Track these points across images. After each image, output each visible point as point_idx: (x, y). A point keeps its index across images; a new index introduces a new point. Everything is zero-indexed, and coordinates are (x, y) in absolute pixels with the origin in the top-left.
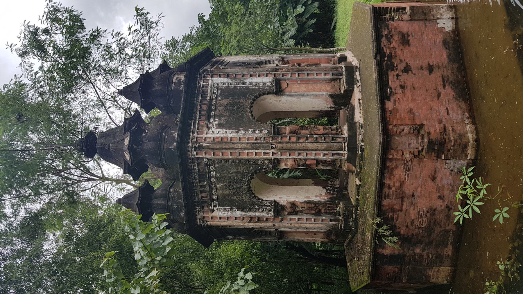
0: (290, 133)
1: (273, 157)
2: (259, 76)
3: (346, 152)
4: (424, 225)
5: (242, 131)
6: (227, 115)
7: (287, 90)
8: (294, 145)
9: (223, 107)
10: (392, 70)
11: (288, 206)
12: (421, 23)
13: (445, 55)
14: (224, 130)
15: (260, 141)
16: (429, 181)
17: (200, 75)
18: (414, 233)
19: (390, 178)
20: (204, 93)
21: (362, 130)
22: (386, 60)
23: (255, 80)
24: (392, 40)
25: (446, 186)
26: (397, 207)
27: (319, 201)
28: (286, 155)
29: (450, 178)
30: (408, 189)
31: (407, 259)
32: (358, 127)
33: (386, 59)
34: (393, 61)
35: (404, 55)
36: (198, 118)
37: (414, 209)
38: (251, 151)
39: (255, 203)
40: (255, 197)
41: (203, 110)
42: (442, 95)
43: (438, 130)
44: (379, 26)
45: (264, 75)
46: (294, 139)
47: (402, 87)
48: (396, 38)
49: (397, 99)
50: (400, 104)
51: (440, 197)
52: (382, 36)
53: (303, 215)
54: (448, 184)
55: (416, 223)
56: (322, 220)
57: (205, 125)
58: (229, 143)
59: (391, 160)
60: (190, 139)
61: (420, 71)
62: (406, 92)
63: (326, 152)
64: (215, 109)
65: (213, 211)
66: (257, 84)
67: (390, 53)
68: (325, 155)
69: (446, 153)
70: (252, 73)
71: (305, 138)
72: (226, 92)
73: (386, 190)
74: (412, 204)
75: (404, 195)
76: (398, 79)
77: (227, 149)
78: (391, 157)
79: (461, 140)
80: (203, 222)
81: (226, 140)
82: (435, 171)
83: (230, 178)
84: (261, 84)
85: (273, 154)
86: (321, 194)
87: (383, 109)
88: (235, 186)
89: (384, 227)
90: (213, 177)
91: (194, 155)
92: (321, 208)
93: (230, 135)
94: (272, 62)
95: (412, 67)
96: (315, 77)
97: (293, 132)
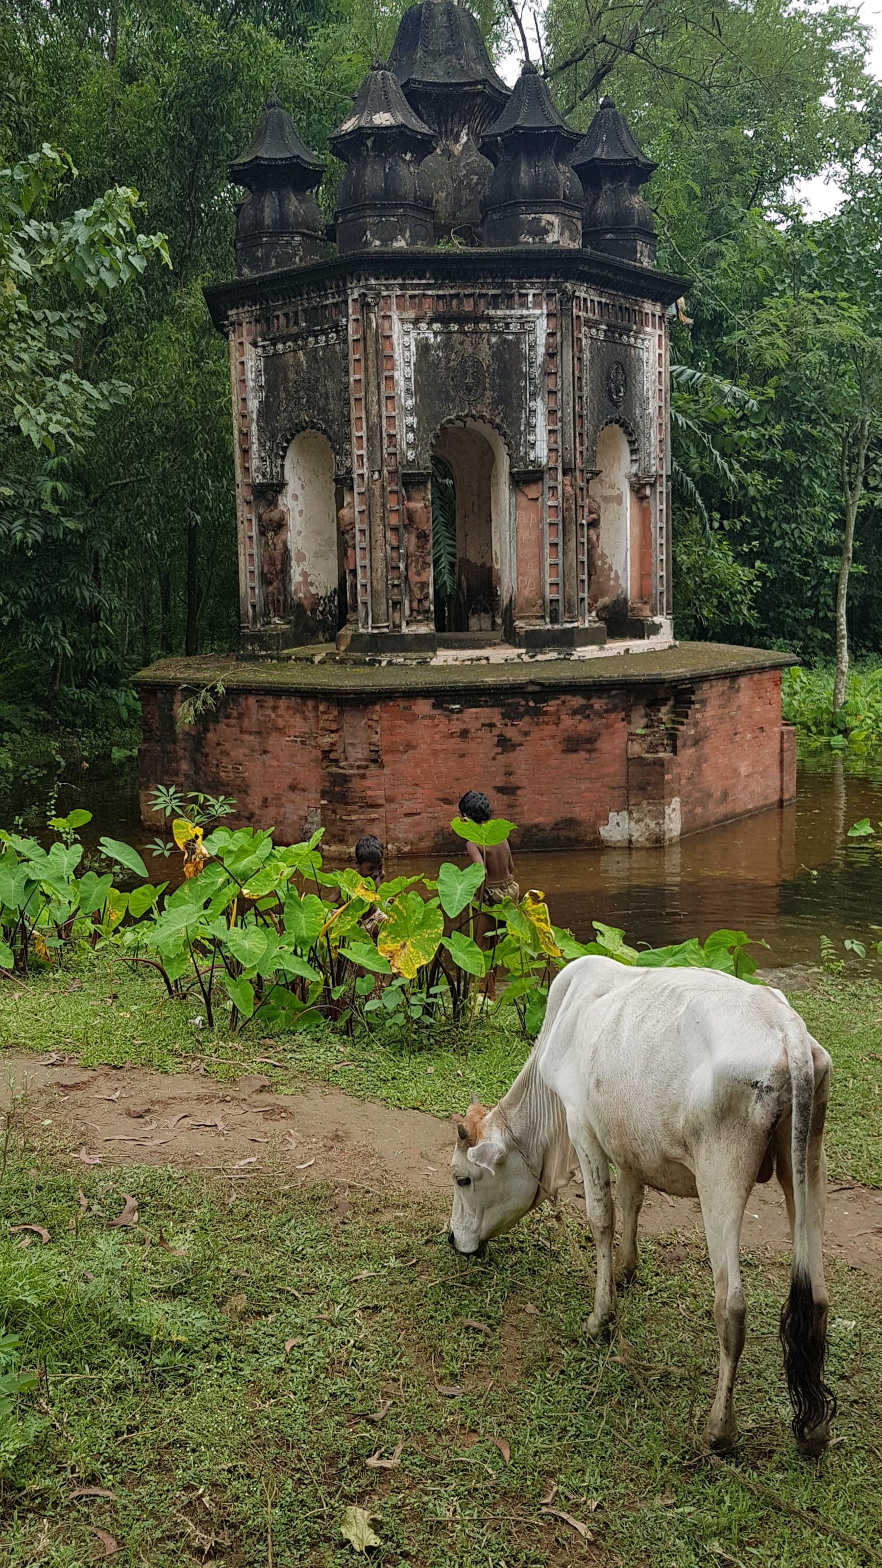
0: (408, 510)
1: (355, 476)
2: (550, 431)
3: (370, 630)
4: (222, 774)
5: (410, 403)
6: (452, 363)
7: (523, 501)
8: (378, 521)
9: (470, 350)
10: (504, 716)
11: (275, 515)
12: (621, 780)
13: (540, 820)
14: (413, 360)
15: (385, 446)
16: (288, 781)
17: (555, 285)
18: (209, 758)
19: (288, 708)
20: (507, 299)
21: (414, 663)
22: (527, 704)
23: (541, 422)
24: (579, 717)
25: (283, 810)
26: (246, 723)
27: (290, 580)
28: (360, 504)
29: (295, 818)
30: (274, 742)
31: (170, 747)
32: (423, 655)
33: (531, 704)
34: (526, 719)
35: (539, 741)
36: (440, 292)
37: (245, 755)
38: (364, 425)
39: (278, 440)
40: (288, 441)
41: (461, 302)
42: (446, 806)
43: (369, 793)
44: (614, 692)
45: (555, 442)
46: (394, 520)
47: (464, 734)
48: (584, 727)
49: (436, 721)
50: (426, 727)
51: (265, 800)
52: (589, 699)
53: (259, 546)
54: (285, 814)
55: (225, 760)
56: (253, 588)
57: (422, 313)
58: (378, 375)
59: (316, 708)
60: (386, 279)
61: (502, 770)
62: (453, 741)
63: (369, 588)
64: (465, 333)
65: (255, 345)
66: (531, 428)
67: (546, 713)
68: (364, 586)
69: (330, 807)
70: (559, 414)
71: (395, 544)
72: (510, 355)
73: (270, 701)
74: (252, 751)
75: (265, 735)
76: (483, 725)
77: (366, 370)
78: (322, 708)
79: (352, 832)
80: (232, 324)
81: (386, 365)
82: (304, 790)
83: (317, 380)
84: (531, 438)
85: (361, 476)
86: (312, 584)
87: (413, 694)
88: (302, 394)
89: (210, 701)
90: (317, 342)
91: (352, 293)
92: (275, 584)
93: (397, 375)
94: (634, 457)
95: (511, 755)
96: (548, 561)
97: (410, 515)
